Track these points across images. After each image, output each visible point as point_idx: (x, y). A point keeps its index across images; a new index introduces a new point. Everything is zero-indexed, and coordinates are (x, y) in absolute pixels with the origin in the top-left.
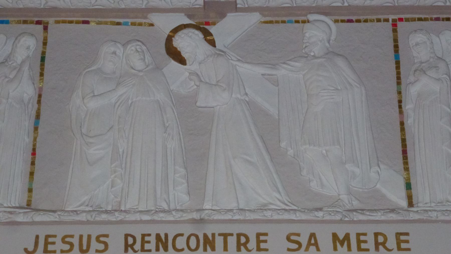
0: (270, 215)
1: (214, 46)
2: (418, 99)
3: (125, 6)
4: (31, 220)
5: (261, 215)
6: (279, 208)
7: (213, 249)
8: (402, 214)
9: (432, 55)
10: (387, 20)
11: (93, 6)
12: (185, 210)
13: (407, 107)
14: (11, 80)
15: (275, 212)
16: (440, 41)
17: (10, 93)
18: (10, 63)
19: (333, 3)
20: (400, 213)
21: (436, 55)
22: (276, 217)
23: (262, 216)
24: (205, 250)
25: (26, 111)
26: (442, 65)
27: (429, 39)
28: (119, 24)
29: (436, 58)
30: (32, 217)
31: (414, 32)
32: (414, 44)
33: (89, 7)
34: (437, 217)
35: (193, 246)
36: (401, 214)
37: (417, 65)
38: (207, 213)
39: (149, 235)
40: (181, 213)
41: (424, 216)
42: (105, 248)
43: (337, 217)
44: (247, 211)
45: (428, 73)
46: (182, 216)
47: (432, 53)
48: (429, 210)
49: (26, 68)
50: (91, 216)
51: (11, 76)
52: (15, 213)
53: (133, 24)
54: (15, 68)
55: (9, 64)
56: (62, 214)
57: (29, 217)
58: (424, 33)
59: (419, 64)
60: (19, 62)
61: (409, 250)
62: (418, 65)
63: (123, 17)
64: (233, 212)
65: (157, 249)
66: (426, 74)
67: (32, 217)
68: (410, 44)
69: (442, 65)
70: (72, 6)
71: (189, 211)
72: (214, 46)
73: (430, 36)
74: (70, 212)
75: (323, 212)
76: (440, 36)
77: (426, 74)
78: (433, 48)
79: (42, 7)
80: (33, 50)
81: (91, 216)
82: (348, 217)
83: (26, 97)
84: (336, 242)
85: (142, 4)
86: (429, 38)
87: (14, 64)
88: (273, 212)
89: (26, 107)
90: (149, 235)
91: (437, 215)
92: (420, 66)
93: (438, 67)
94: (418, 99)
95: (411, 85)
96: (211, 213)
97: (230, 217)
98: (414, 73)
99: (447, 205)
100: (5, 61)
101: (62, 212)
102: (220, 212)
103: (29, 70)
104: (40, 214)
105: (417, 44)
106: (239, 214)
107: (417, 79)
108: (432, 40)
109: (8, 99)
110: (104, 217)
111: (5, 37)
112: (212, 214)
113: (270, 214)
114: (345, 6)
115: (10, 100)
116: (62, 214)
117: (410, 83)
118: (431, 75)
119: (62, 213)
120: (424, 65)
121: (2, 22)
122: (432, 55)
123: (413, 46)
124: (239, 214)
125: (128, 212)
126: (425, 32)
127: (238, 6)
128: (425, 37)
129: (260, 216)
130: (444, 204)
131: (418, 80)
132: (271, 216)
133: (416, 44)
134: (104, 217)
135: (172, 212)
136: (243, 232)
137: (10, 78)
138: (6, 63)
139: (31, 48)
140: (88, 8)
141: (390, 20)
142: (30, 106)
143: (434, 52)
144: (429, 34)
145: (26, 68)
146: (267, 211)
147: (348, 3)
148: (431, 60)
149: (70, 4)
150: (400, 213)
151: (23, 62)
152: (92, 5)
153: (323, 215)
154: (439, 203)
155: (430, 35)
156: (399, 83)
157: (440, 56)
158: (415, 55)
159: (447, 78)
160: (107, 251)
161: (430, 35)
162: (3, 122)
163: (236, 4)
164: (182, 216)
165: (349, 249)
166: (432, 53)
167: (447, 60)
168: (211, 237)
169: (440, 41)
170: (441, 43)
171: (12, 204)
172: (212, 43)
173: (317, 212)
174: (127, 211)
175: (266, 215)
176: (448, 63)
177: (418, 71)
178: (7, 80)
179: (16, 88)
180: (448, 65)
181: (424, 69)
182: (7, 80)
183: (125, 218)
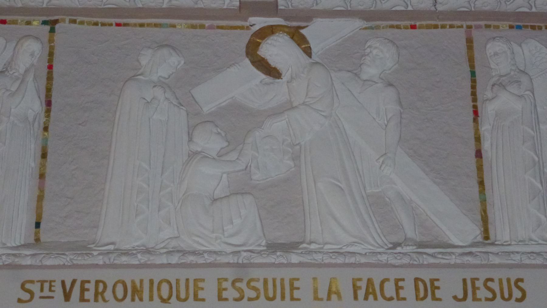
0: (320, 259)
1: (310, 57)
2: (496, 118)
3: (143, 5)
4: (40, 264)
5: (309, 259)
6: (367, 248)
7: (141, 300)
8: (480, 257)
9: (513, 68)
10: (461, 27)
11: (104, 5)
12: (219, 252)
13: (483, 129)
14: (13, 94)
15: (326, 255)
16: (523, 51)
17: (12, 110)
18: (11, 73)
19: (396, 6)
20: (478, 256)
21: (517, 67)
22: (327, 261)
23: (311, 259)
24: (133, 300)
25: (32, 132)
26: (524, 79)
27: (510, 49)
28: (126, 25)
29: (518, 70)
30: (41, 261)
31: (492, 40)
32: (492, 54)
33: (100, 6)
34: (521, 261)
35: (120, 295)
36: (479, 257)
37: (495, 79)
38: (245, 256)
39: (89, 282)
40: (215, 256)
41: (372, 260)
42: (520, 298)
43: (403, 260)
44: (356, 254)
45: (508, 88)
46: (149, 260)
47: (513, 65)
48: (382, 252)
49: (30, 78)
50: (109, 259)
51: (13, 89)
52: (21, 255)
53: (118, 25)
54: (17, 79)
55: (10, 74)
56: (75, 258)
57: (38, 261)
58: (504, 41)
59: (498, 78)
60: (22, 71)
61: (356, 298)
62: (496, 79)
63: (132, 17)
64: (276, 255)
65: (96, 300)
66: (505, 89)
67: (41, 261)
68: (488, 54)
69: (524, 79)
70: (79, 4)
71: (224, 253)
72: (310, 57)
73: (510, 45)
74: (85, 256)
75: (387, 255)
76: (523, 45)
77: (505, 89)
78: (514, 58)
79: (45, 6)
80: (38, 56)
81: (109, 259)
82: (417, 259)
83: (31, 115)
84: (69, 291)
85: (163, 3)
86: (510, 47)
87: (16, 74)
88: (389, 256)
89: (32, 126)
90: (89, 282)
91: (521, 258)
92: (498, 80)
93: (520, 81)
94: (496, 118)
95: (488, 101)
96: (251, 256)
97: (273, 261)
98: (492, 88)
99: (530, 244)
100: (5, 69)
101: (75, 255)
102: (261, 255)
103: (34, 81)
104: (51, 257)
105: (496, 54)
106: (284, 257)
107: (495, 95)
108: (513, 49)
109: (9, 117)
110: (124, 259)
111: (5, 41)
112: (252, 257)
113: (321, 258)
114: (409, 10)
115: (12, 118)
116: (75, 258)
117: (486, 100)
118: (511, 91)
119: (75, 256)
120: (504, 78)
121: (4, 22)
122: (513, 68)
123: (490, 56)
124: (283, 257)
125: (153, 253)
126: (505, 40)
127: (280, 7)
128: (505, 46)
129: (372, 260)
130: (527, 243)
131: (497, 96)
132: (322, 259)
133: (494, 53)
134: (124, 259)
135: (137, 255)
136: (422, 278)
137: (12, 91)
138: (7, 72)
139: (36, 54)
140: (99, 7)
141: (465, 26)
142: (36, 124)
143: (515, 64)
144: (510, 43)
145: (30, 78)
146: (316, 254)
147: (412, 6)
148: (512, 73)
149: (77, 3)
150: (478, 256)
151: (27, 71)
152: (104, 3)
153: (388, 258)
154: (520, 241)
155: (511, 44)
156: (475, 100)
157: (521, 69)
158: (492, 67)
159: (530, 95)
160: (492, 302)
161: (511, 44)
162: (5, 144)
163: (277, 6)
164: (149, 260)
165: (376, 299)
166: (513, 65)
167: (531, 74)
168: (419, 284)
169: (523, 51)
170: (523, 54)
171: (16, 243)
172: (308, 52)
173: (513, 255)
174: (152, 252)
175: (316, 258)
176: (532, 77)
177: (496, 86)
178: (8, 93)
179: (20, 103)
180: (531, 79)
181: (503, 84)
182: (8, 93)
183: (216, 260)
